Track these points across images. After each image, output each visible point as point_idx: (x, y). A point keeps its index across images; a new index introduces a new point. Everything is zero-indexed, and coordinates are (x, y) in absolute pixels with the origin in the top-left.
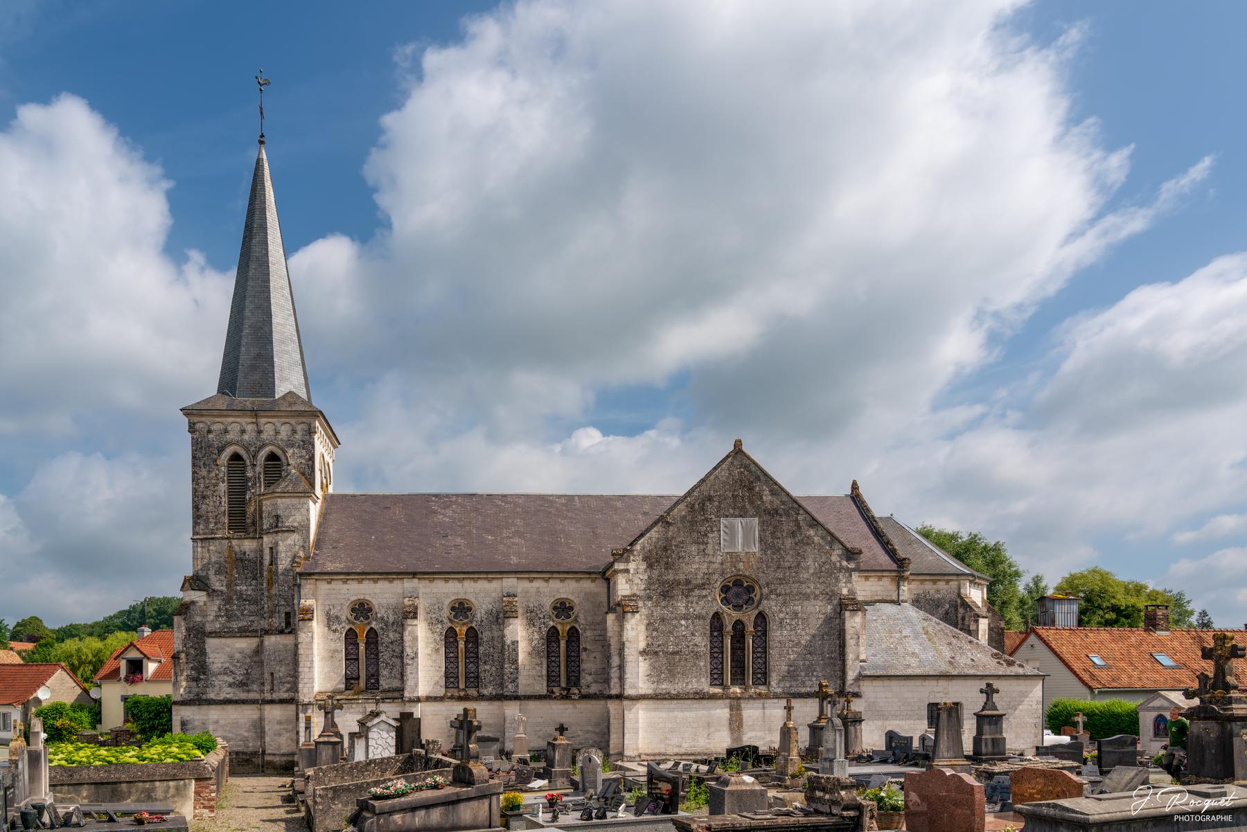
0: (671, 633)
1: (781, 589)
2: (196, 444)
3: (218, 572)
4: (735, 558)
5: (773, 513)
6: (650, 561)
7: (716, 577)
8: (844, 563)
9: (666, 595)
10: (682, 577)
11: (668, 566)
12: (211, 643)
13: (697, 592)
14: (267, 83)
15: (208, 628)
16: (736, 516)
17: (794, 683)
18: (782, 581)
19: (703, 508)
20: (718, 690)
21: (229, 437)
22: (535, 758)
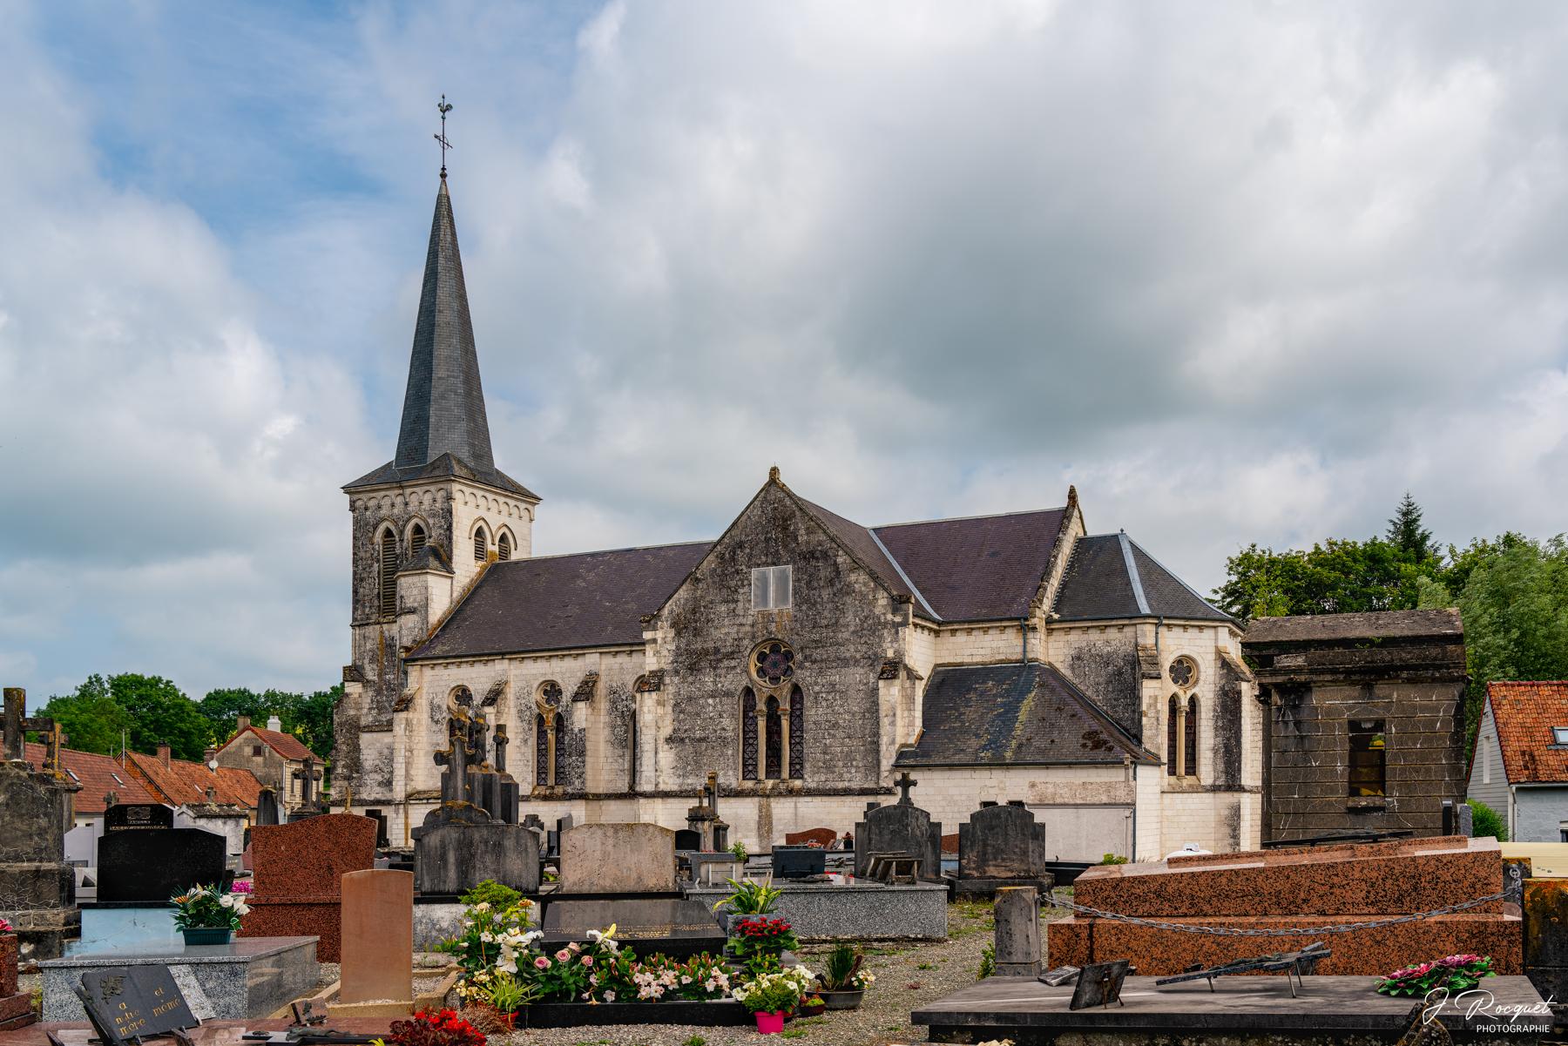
0: (698, 714)
1: (817, 654)
2: (356, 522)
3: (372, 661)
4: (768, 618)
5: (810, 556)
6: (679, 627)
7: (746, 642)
8: (889, 617)
9: (693, 668)
10: (710, 645)
11: (697, 633)
12: (365, 738)
13: (726, 663)
14: (449, 108)
15: (363, 722)
16: (768, 565)
17: (830, 776)
18: (818, 644)
19: (733, 559)
20: (749, 784)
21: (384, 512)
22: (1474, 936)
